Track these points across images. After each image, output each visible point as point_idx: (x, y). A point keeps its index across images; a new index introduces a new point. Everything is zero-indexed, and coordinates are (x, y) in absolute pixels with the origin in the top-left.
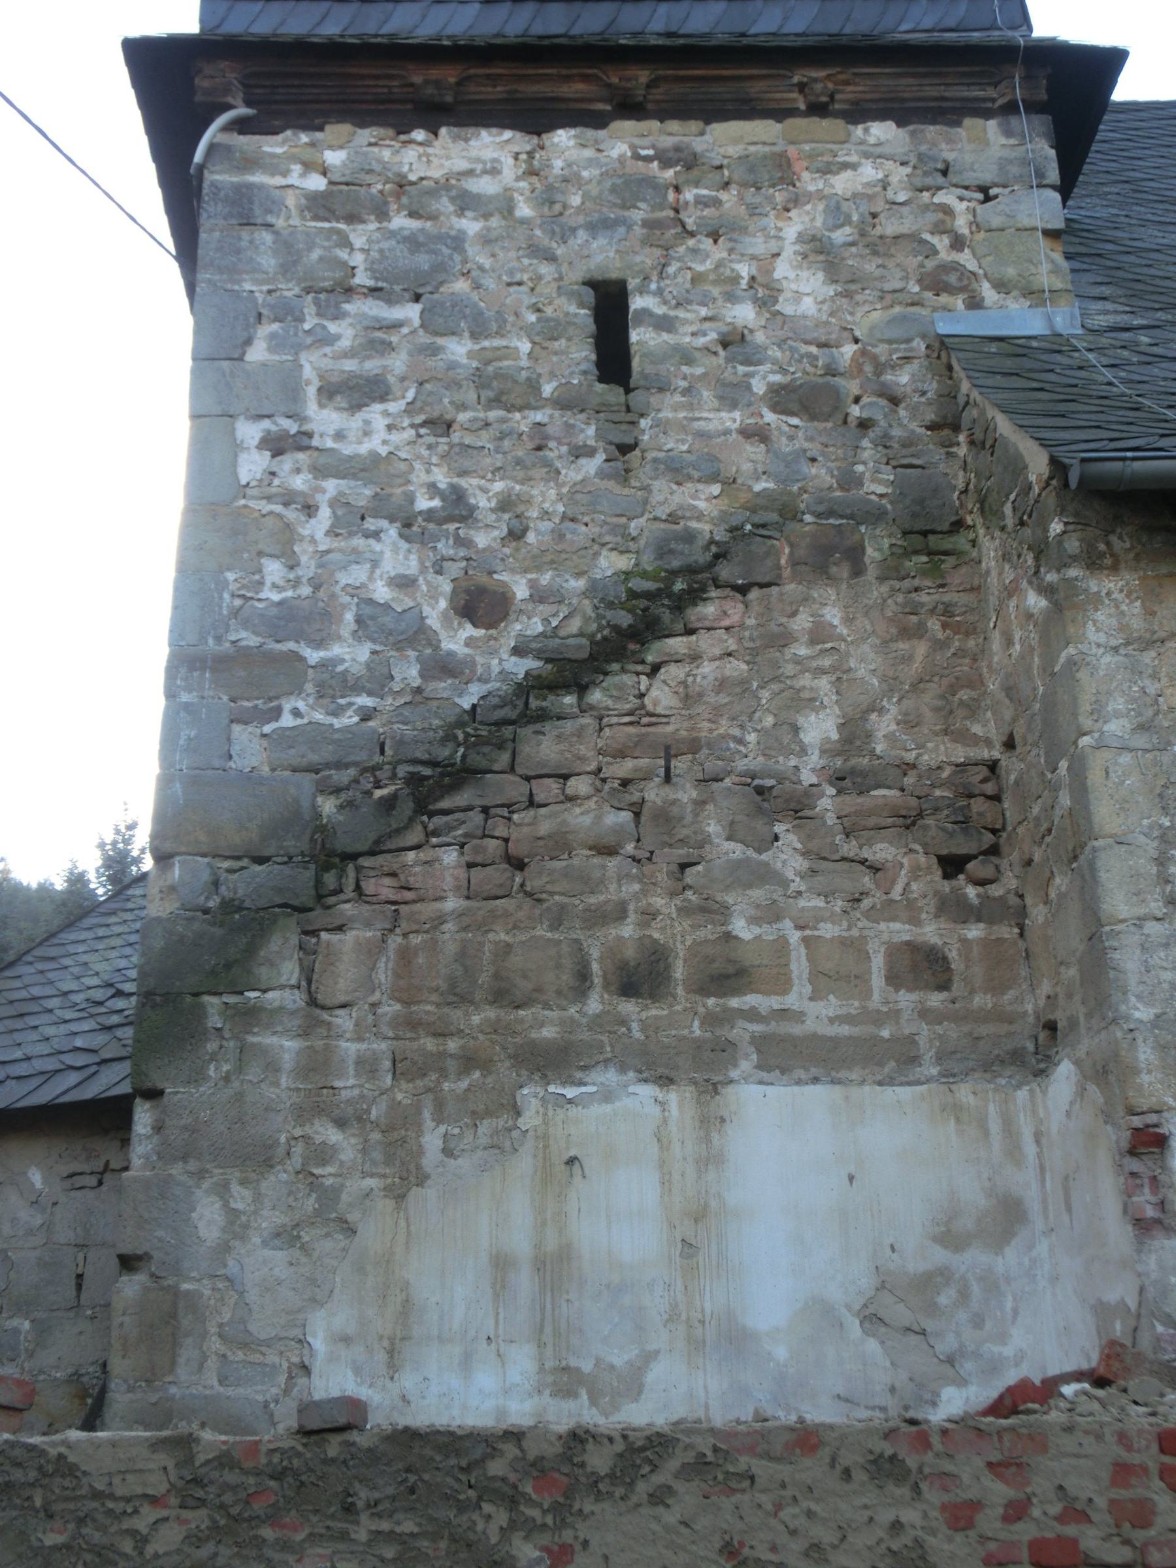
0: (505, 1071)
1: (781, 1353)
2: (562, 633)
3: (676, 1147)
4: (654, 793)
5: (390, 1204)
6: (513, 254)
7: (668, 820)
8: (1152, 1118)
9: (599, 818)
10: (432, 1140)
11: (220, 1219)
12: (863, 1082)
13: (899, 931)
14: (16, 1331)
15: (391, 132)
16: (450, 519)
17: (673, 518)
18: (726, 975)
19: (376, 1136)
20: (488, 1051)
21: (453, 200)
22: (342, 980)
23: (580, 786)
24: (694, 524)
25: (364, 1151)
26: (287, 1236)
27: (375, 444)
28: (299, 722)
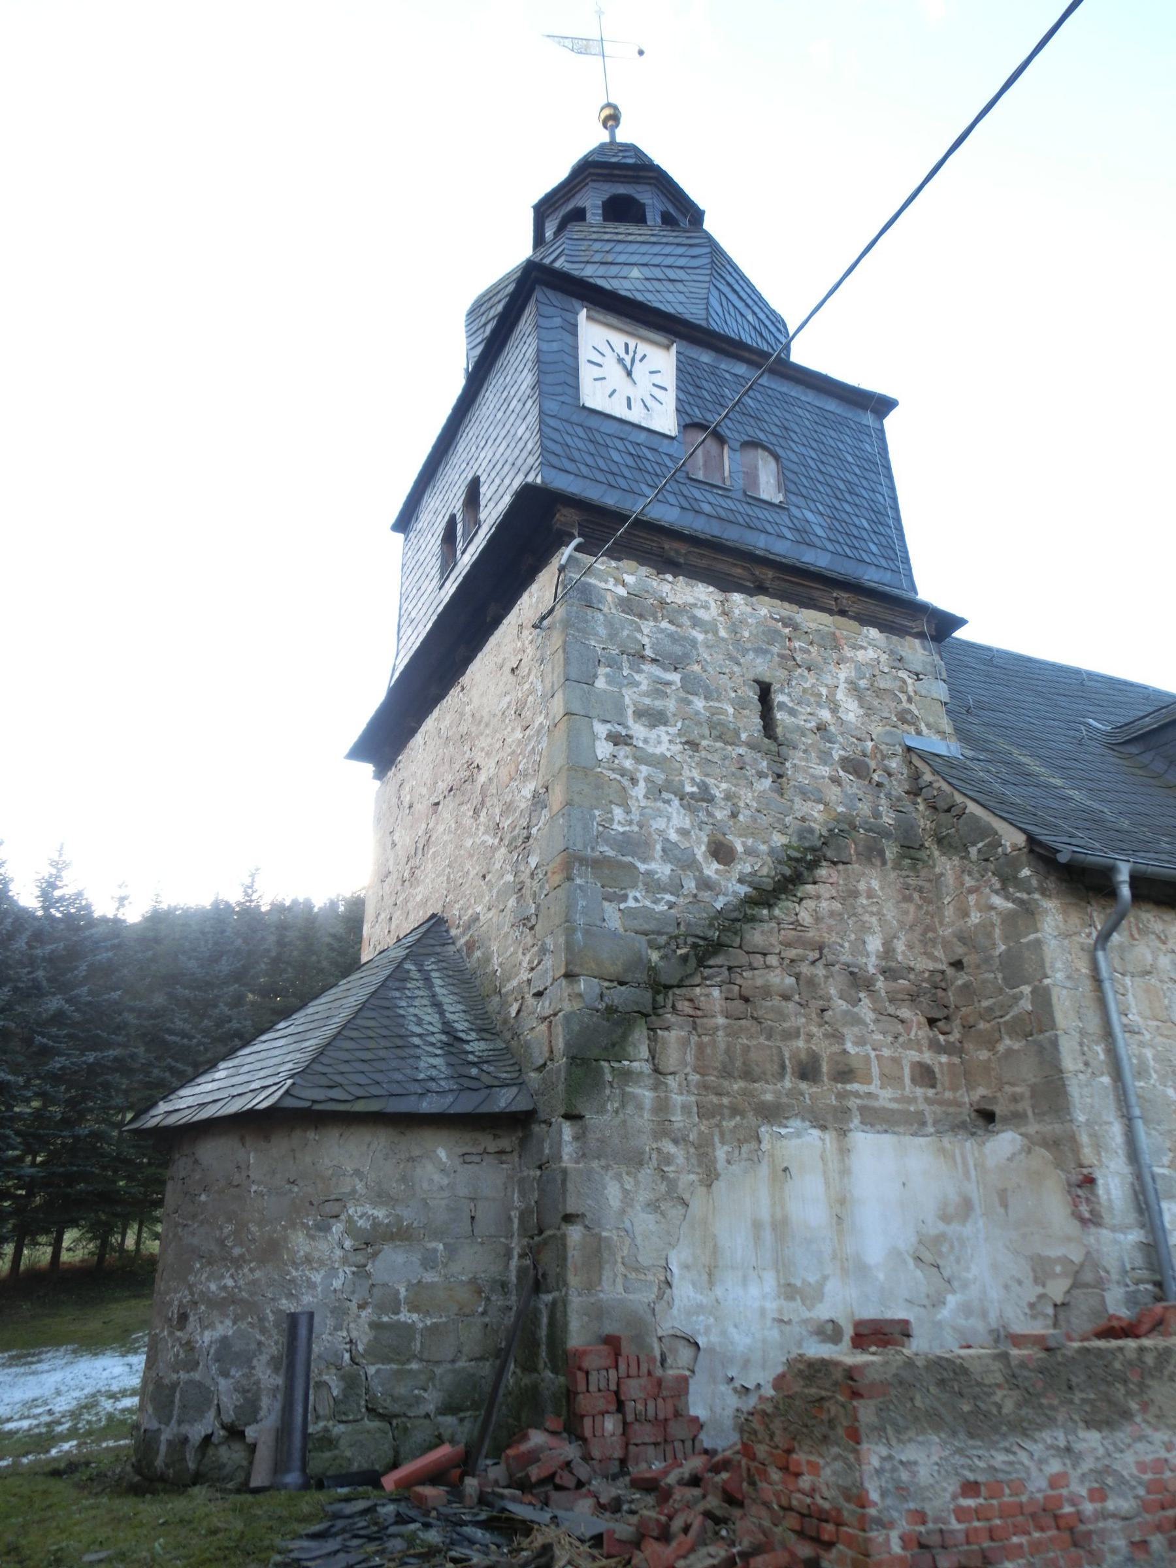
0: (751, 1118)
1: (881, 1277)
2: (759, 874)
3: (830, 1164)
4: (805, 969)
5: (704, 1189)
6: (721, 657)
7: (814, 985)
8: (1090, 1170)
9: (782, 979)
10: (721, 1153)
11: (620, 1195)
12: (905, 1134)
13: (913, 1055)
14: (435, 1250)
15: (655, 572)
16: (703, 800)
17: (803, 819)
18: (845, 1074)
19: (692, 1150)
20: (743, 1105)
21: (689, 618)
22: (671, 1058)
23: (773, 960)
24: (813, 824)
25: (687, 1159)
26: (653, 1206)
27: (663, 749)
28: (638, 905)
